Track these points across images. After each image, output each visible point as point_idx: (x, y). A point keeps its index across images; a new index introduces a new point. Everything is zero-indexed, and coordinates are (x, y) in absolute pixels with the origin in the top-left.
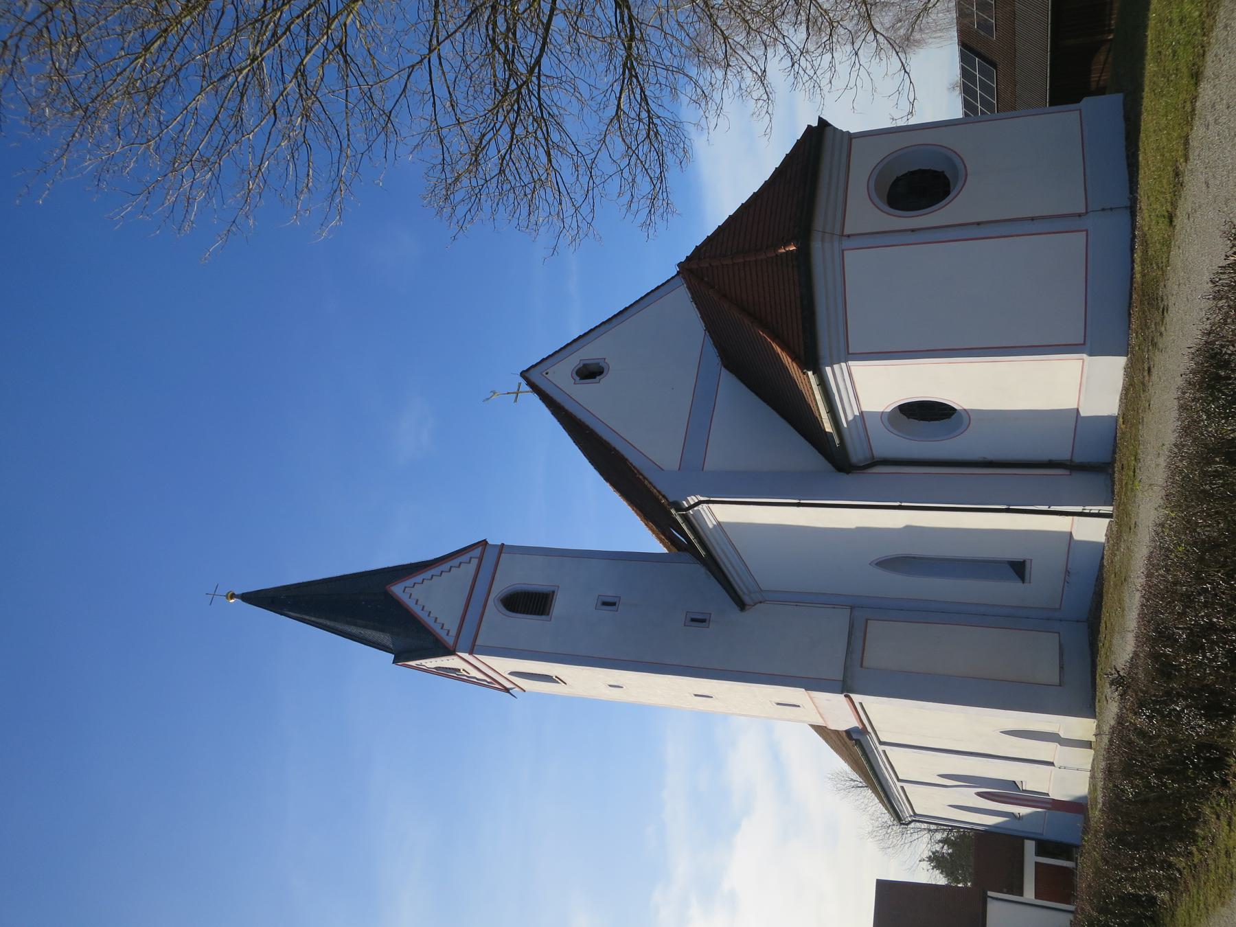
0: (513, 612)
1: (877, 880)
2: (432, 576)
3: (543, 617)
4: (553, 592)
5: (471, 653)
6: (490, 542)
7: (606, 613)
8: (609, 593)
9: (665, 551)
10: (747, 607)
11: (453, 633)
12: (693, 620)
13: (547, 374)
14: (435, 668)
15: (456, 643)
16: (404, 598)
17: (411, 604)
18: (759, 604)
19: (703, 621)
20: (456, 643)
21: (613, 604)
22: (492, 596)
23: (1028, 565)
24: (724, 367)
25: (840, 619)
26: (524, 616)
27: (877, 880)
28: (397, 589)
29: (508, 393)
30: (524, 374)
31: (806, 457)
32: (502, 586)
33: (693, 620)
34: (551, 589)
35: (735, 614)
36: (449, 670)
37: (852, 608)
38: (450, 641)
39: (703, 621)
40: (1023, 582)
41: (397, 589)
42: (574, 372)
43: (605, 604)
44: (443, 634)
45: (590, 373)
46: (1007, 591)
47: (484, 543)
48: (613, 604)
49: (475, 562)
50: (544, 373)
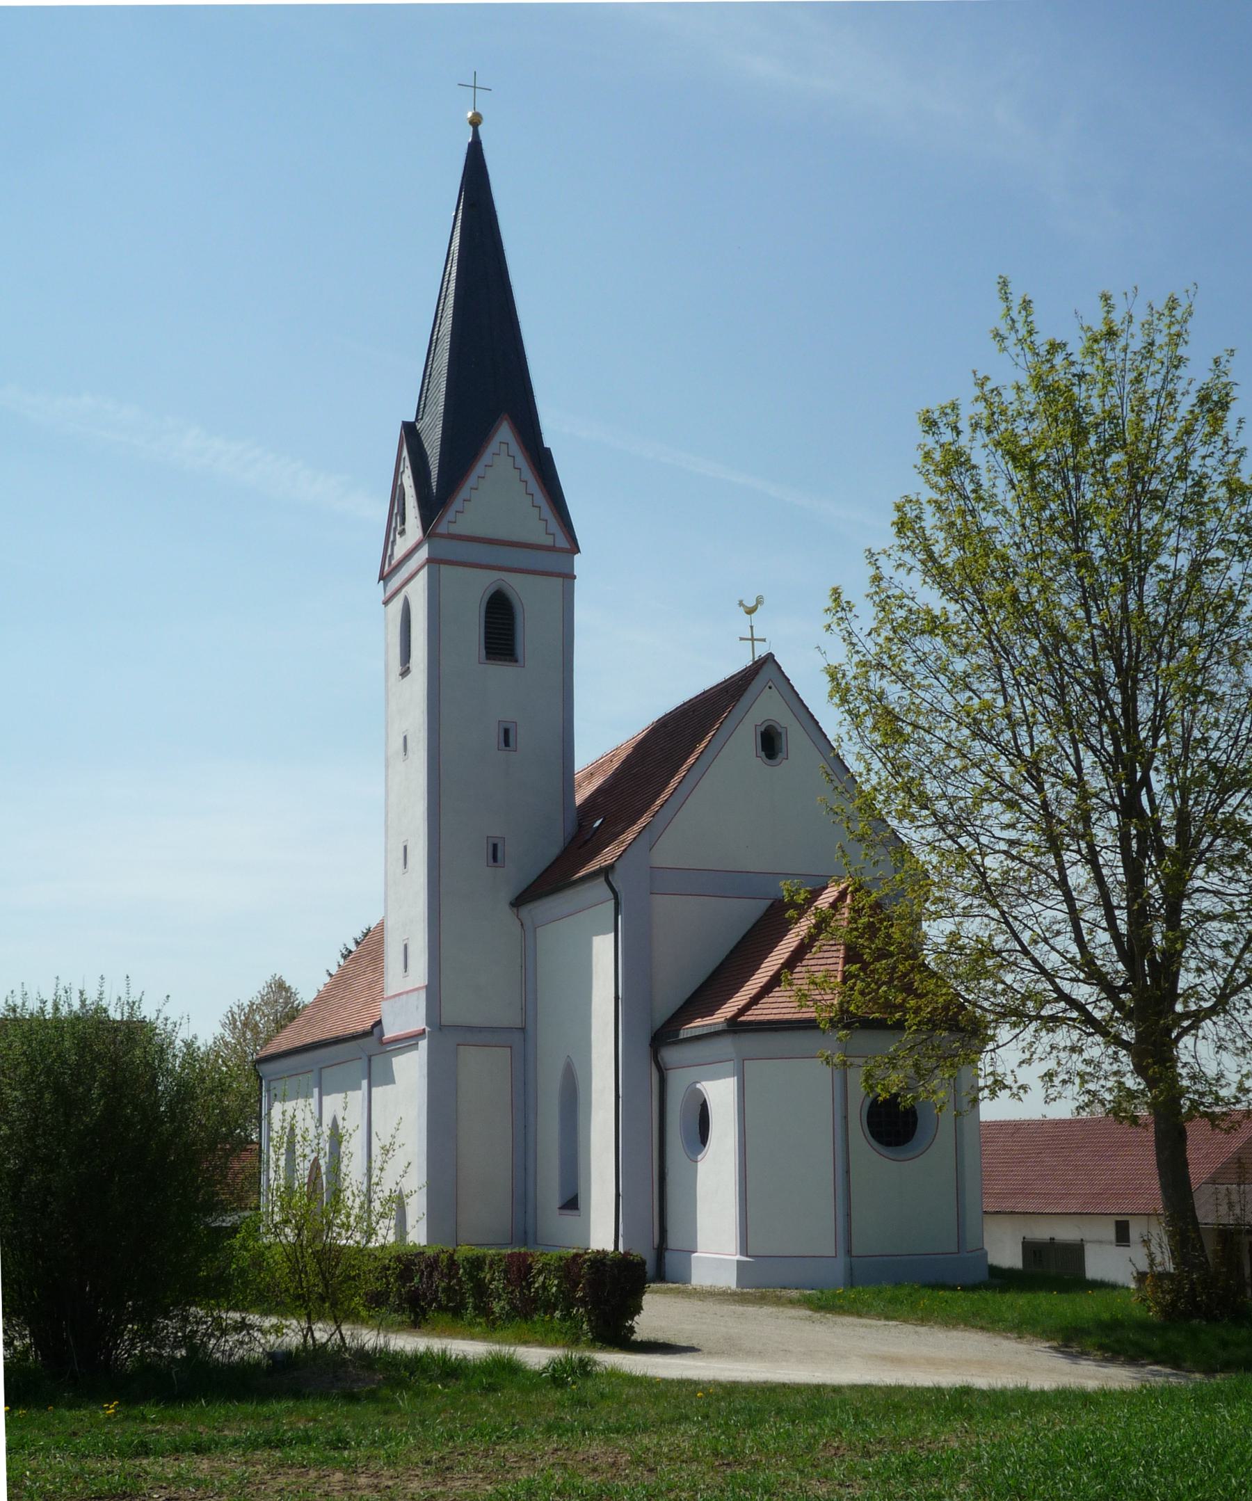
0: (488, 603)
1: (394, 1083)
2: (526, 482)
3: (483, 652)
4: (516, 661)
5: (430, 561)
6: (576, 557)
7: (495, 736)
8: (522, 737)
9: (577, 804)
10: (515, 910)
11: (454, 529)
12: (495, 846)
13: (770, 688)
14: (402, 484)
15: (442, 536)
16: (493, 446)
17: (486, 458)
18: (481, 128)
19: (495, 858)
20: (442, 536)
21: (507, 743)
22: (503, 575)
23: (575, 1212)
24: (772, 905)
25: (510, 1018)
26: (483, 614)
27: (394, 1083)
28: (504, 434)
29: (752, 627)
30: (770, 658)
31: (669, 999)
32: (522, 589)
33: (495, 846)
34: (520, 658)
35: (507, 893)
36: (401, 502)
37: (523, 1029)
38: (442, 529)
39: (495, 858)
40: (560, 1208)
41: (504, 434)
42: (771, 723)
43: (506, 732)
44: (450, 515)
45: (770, 743)
46: (550, 1194)
47: (576, 549)
48: (507, 743)
49: (548, 541)
50: (770, 684)
